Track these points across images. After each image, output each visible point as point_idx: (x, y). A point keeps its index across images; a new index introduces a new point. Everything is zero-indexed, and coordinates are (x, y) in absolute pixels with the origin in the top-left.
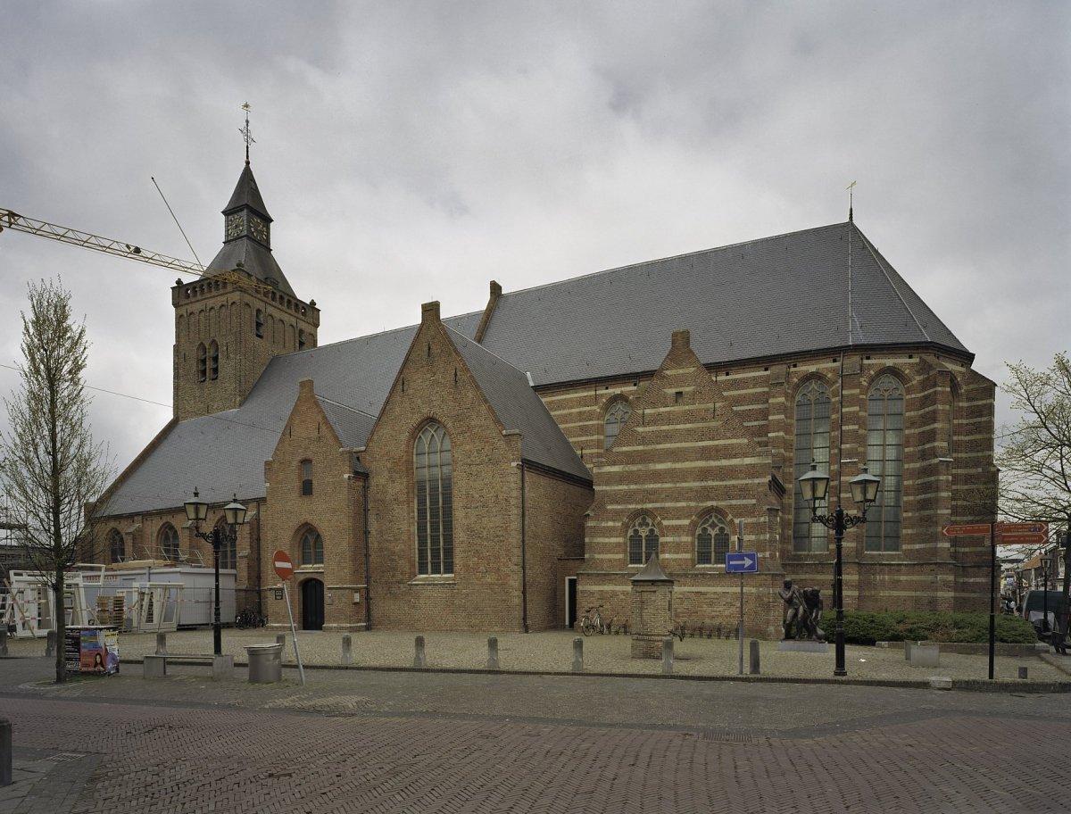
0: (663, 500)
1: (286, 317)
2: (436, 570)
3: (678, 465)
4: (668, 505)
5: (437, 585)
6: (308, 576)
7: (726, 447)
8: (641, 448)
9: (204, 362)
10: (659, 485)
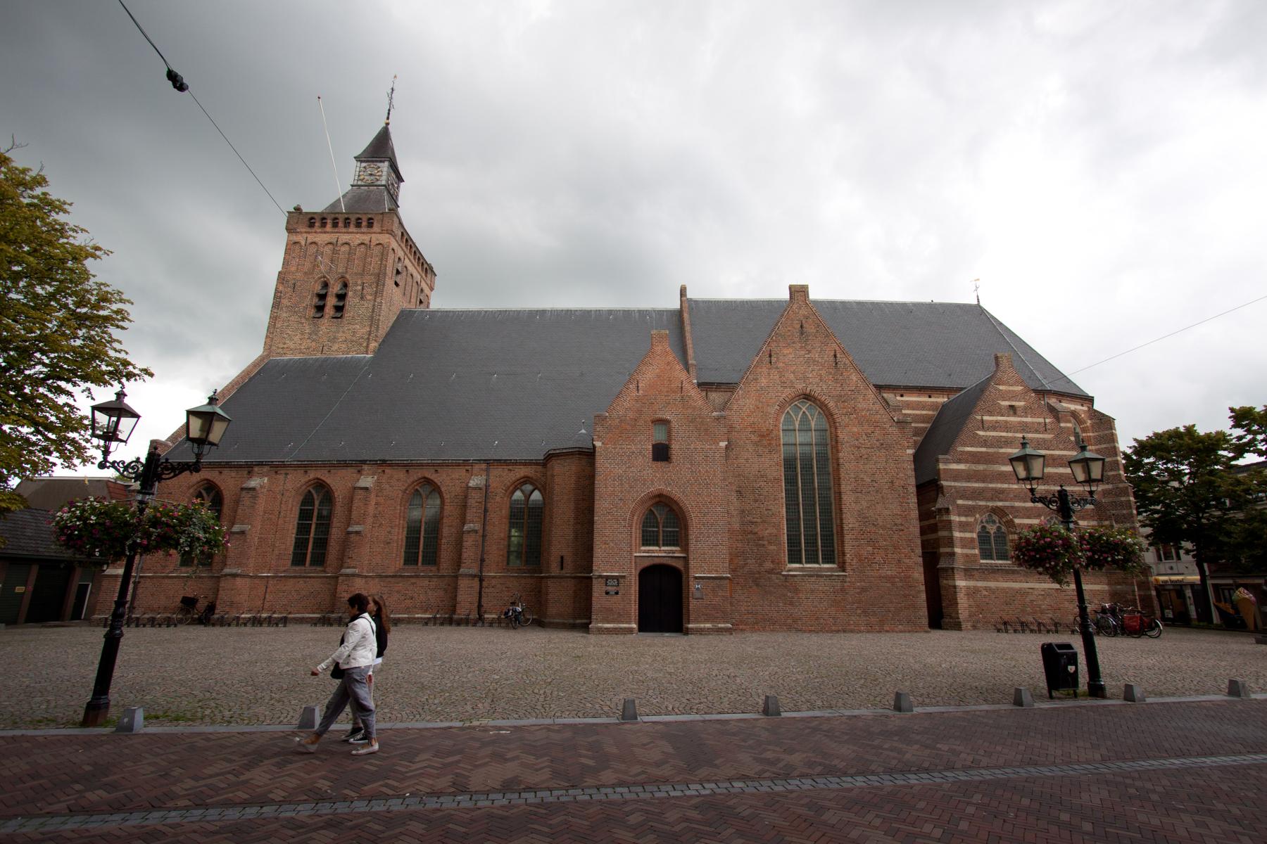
0: (1011, 500)
1: (415, 274)
2: (812, 559)
4: (1017, 504)
5: (821, 576)
6: (657, 561)
8: (984, 450)
9: (322, 297)
10: (1006, 486)
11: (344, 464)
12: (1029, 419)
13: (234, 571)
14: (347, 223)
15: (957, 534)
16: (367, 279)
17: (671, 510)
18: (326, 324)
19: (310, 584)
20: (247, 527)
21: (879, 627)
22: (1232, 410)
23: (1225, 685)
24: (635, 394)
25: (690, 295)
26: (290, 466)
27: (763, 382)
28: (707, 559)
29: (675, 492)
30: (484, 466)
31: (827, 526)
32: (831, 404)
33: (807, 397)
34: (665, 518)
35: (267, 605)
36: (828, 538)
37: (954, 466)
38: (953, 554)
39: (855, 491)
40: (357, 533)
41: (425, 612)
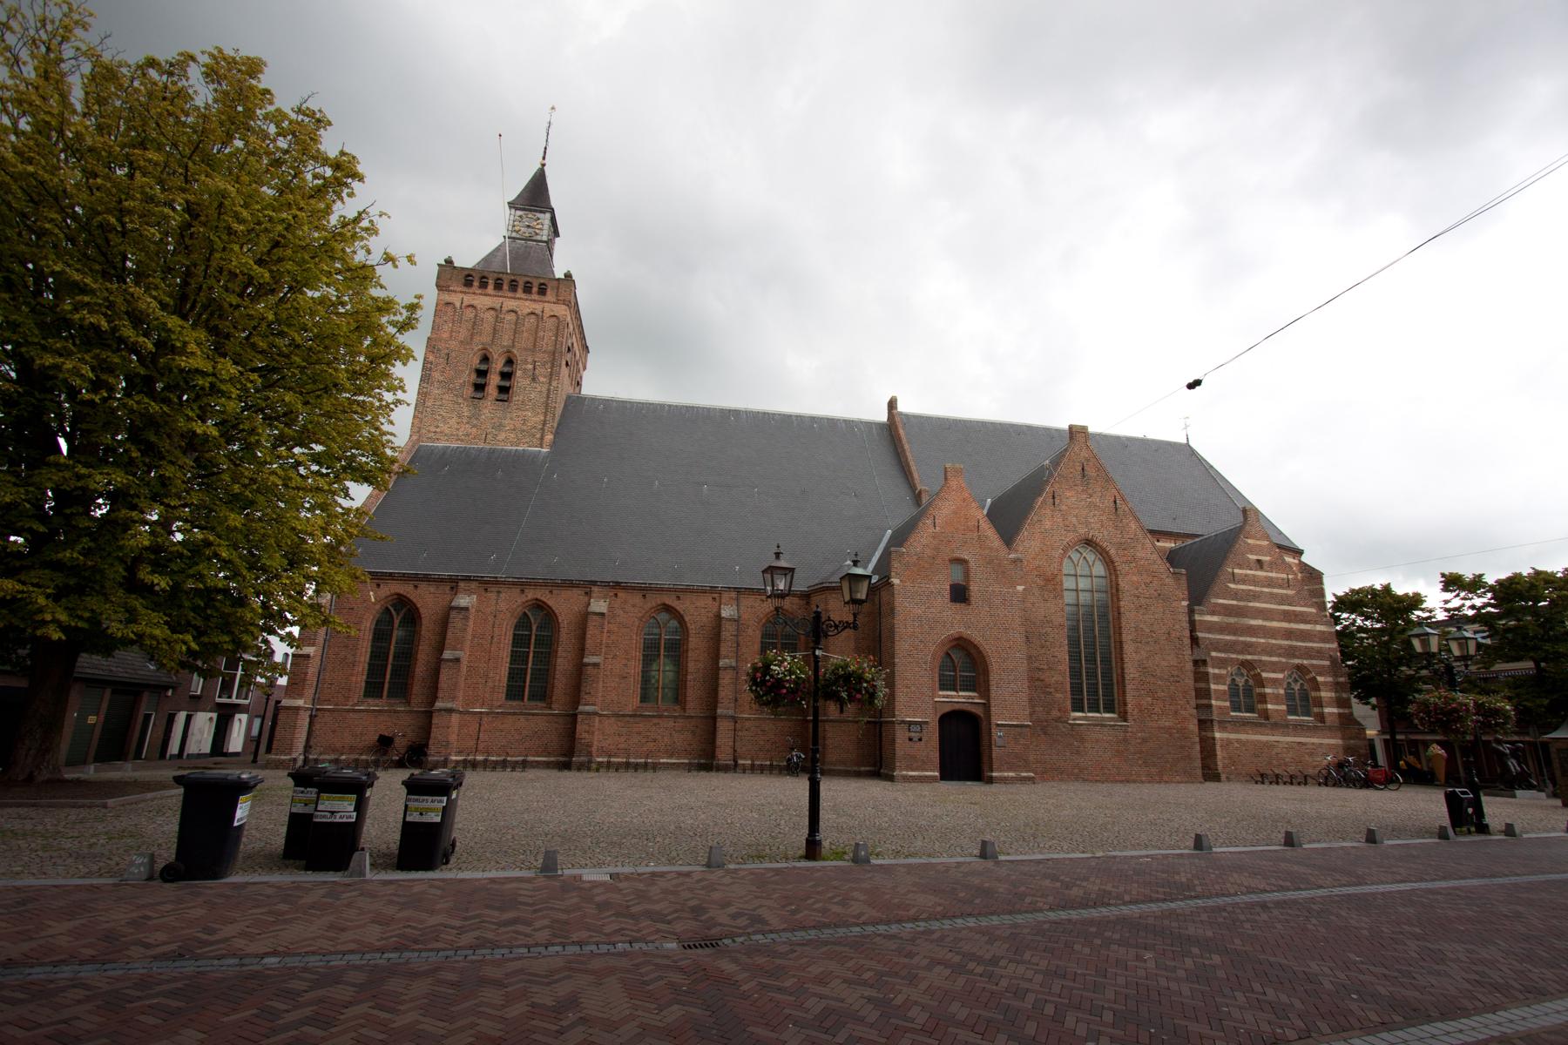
3: (1268, 624)
4: (1264, 658)
6: (957, 707)
7: (1302, 613)
9: (482, 373)
11: (570, 584)
12: (1273, 575)
13: (449, 705)
14: (513, 286)
15: (1213, 687)
16: (539, 357)
17: (969, 654)
18: (489, 407)
19: (536, 723)
20: (458, 653)
21: (1159, 777)
22: (1443, 575)
23: (1281, 836)
24: (931, 530)
25: (902, 407)
26: (504, 583)
27: (1047, 524)
28: (1008, 707)
29: (975, 636)
30: (734, 595)
31: (1107, 674)
32: (1112, 552)
33: (1089, 543)
34: (965, 662)
35: (481, 746)
36: (1108, 687)
37: (1208, 618)
38: (1210, 706)
39: (1134, 641)
40: (596, 665)
41: (671, 756)
